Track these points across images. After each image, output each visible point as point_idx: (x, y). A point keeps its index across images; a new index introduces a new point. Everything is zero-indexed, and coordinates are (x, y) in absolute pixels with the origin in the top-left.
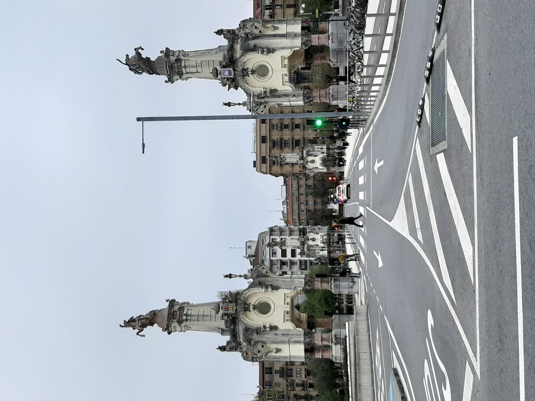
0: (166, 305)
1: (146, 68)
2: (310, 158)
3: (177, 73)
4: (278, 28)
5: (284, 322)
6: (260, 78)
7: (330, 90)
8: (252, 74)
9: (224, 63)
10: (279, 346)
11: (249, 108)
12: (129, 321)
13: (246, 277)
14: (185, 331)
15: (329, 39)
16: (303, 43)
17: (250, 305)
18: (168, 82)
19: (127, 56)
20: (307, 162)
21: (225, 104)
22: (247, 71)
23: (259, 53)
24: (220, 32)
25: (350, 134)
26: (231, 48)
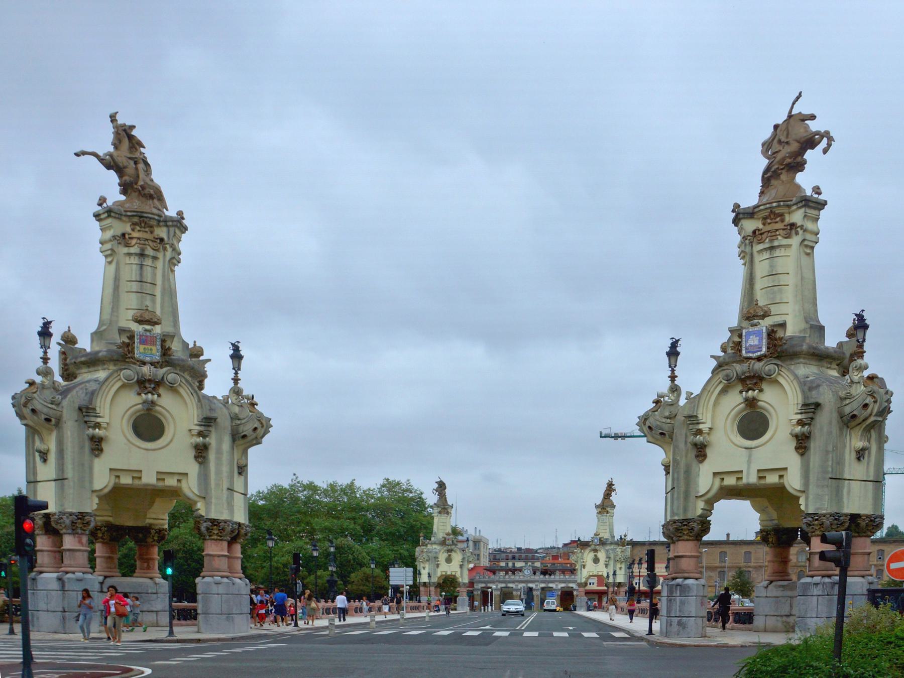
0: (171, 212)
1: (778, 162)
2: (602, 555)
5: (111, 469)
6: (735, 420)
7: (697, 579)
8: (746, 400)
9: (780, 334)
10: (52, 457)
11: (662, 399)
12: (131, 138)
13: (237, 391)
14: (102, 252)
15: (823, 576)
17: (153, 394)
18: (733, 211)
19: (813, 117)
20: (595, 551)
21: (674, 345)
22: (154, 393)
24: (860, 325)
26: (821, 356)
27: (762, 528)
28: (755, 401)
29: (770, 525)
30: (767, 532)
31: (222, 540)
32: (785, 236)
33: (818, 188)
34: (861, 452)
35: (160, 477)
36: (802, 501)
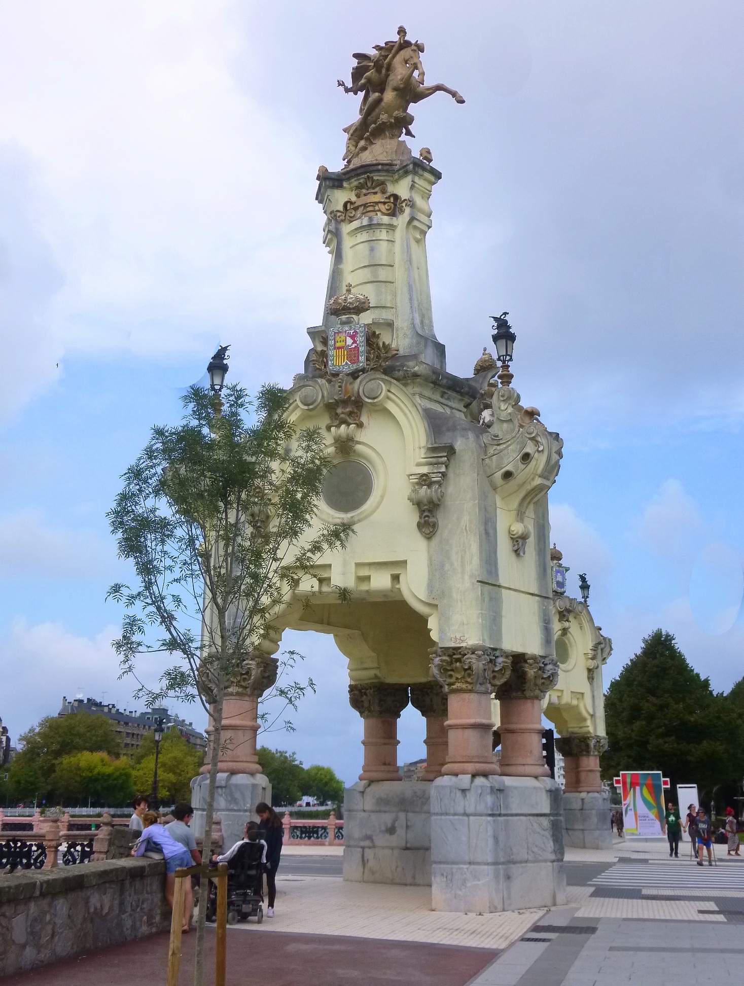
3: (352, 203)
4: (517, 552)
16: (455, 654)
17: (348, 424)
22: (350, 421)
23: (419, 465)
25: (674, 855)
27: (353, 683)
28: (350, 443)
29: (367, 675)
30: (360, 691)
31: (471, 691)
32: (386, 212)
33: (429, 152)
34: (520, 541)
35: (364, 572)
36: (432, 624)
